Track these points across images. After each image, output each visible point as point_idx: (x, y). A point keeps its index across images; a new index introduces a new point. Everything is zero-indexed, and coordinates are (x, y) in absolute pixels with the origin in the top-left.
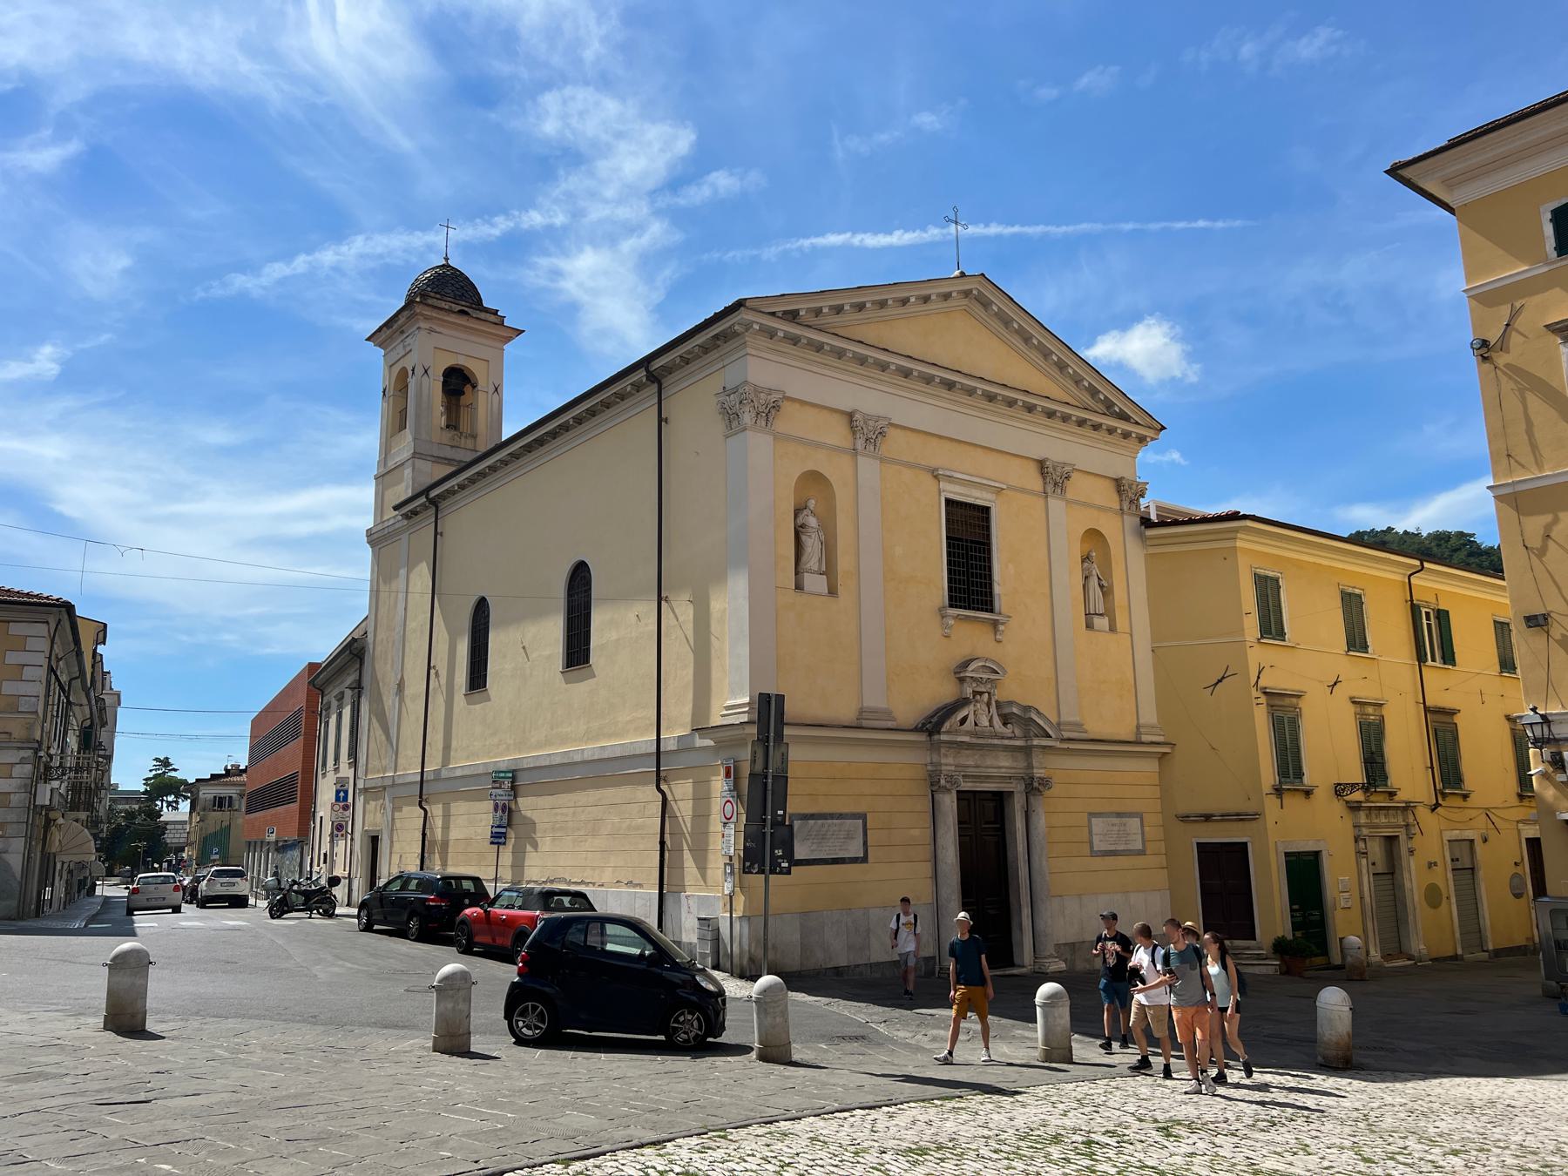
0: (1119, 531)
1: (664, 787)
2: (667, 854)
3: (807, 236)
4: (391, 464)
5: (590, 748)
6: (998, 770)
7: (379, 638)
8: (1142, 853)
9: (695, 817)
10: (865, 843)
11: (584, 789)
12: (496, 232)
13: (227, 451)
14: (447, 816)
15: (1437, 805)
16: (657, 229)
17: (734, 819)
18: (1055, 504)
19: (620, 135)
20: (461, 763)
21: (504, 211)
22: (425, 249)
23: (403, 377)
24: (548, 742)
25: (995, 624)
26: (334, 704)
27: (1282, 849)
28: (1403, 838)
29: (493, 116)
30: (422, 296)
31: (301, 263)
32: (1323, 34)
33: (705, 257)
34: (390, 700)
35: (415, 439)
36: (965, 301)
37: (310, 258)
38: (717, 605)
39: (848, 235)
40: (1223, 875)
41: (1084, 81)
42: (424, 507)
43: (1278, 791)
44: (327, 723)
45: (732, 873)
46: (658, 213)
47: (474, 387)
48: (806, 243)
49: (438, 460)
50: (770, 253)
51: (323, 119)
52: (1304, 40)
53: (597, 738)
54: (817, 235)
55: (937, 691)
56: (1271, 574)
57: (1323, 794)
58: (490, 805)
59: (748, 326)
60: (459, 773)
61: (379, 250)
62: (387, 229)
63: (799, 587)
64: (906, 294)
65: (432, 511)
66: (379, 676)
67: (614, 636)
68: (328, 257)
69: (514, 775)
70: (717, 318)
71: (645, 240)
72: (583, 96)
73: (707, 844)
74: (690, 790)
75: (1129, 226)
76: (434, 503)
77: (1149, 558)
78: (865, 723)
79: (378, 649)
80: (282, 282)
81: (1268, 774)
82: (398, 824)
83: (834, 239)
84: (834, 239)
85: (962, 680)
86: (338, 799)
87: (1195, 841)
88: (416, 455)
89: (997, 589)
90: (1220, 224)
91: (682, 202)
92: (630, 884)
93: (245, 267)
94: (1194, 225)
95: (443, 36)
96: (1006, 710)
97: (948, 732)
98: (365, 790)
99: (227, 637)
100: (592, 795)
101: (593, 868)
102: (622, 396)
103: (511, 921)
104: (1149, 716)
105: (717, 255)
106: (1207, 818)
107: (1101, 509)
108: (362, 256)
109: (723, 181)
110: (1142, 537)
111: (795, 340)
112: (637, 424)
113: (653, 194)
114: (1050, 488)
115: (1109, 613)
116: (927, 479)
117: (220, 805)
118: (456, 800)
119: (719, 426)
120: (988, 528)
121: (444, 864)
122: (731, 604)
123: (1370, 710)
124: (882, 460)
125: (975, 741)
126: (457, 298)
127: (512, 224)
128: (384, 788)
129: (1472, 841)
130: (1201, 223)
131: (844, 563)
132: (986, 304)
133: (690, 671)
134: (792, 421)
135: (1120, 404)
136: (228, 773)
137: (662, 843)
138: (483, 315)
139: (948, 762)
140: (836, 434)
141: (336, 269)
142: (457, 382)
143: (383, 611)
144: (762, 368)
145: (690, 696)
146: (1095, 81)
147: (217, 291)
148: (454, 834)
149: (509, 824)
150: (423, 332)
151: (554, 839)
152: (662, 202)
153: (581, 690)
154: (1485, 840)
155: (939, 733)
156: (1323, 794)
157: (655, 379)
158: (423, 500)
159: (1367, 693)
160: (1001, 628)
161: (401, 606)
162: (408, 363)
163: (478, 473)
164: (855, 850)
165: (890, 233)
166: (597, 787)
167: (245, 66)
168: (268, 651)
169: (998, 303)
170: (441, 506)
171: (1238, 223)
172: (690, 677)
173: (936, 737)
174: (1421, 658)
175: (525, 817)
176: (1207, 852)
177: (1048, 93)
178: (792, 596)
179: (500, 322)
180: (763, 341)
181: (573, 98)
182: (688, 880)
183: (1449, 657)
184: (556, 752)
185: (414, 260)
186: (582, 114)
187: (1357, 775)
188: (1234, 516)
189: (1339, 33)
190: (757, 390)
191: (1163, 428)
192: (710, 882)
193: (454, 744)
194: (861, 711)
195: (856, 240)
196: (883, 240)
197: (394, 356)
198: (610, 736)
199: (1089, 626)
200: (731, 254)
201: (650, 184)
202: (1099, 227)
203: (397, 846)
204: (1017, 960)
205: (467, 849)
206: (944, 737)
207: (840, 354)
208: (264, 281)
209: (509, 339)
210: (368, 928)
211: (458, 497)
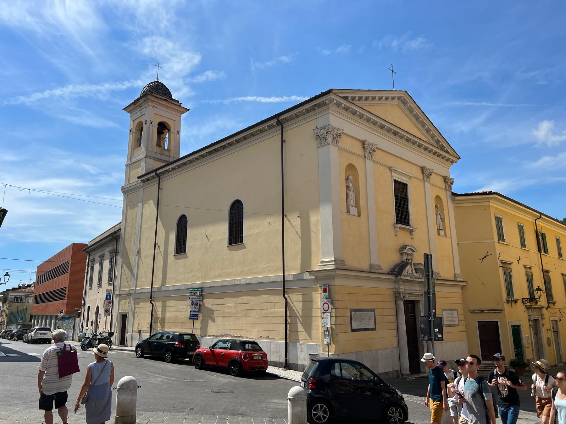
0: (444, 196)
1: (286, 296)
2: (288, 326)
3: (241, 97)
4: (134, 160)
5: (244, 279)
6: (415, 291)
7: (127, 231)
8: (458, 325)
9: (303, 309)
10: (375, 322)
11: (240, 296)
12: (124, 87)
13: (12, 163)
14: (164, 307)
15: (548, 307)
17: (329, 311)
18: (427, 184)
19: (173, 55)
20: (171, 284)
21: (128, 80)
23: (140, 128)
24: (220, 276)
25: (411, 232)
26: (97, 259)
27: (511, 324)
28: (540, 319)
29: (125, 45)
30: (151, 92)
31: (47, 93)
32: (420, 40)
33: (203, 101)
34: (133, 258)
35: (146, 150)
36: (398, 101)
37: (51, 92)
38: (313, 218)
39: (255, 97)
40: (489, 335)
41: (339, 49)
42: (153, 177)
43: (508, 301)
44: (92, 268)
45: (329, 335)
46: (186, 84)
47: (169, 130)
48: (240, 99)
49: (156, 159)
50: (227, 102)
51: (59, 41)
53: (247, 274)
54: (244, 97)
55: (394, 259)
56: (499, 216)
57: (520, 302)
58: (189, 302)
59: (331, 101)
60: (171, 289)
61: (78, 91)
62: (82, 83)
63: (348, 212)
64: (382, 95)
65: (158, 178)
66: (127, 247)
67: (256, 231)
68: (58, 92)
69: (202, 290)
70: (317, 97)
72: (159, 40)
73: (311, 321)
74: (301, 297)
76: (158, 176)
77: (456, 208)
78: (373, 271)
79: (127, 236)
80: (39, 100)
81: (505, 296)
82: (137, 310)
83: (250, 98)
84: (250, 98)
85: (402, 254)
86: (107, 299)
87: (477, 320)
88: (147, 156)
89: (411, 217)
92: (267, 338)
93: (24, 94)
95: (107, 14)
96: (417, 267)
97: (404, 276)
98: (120, 295)
99: (10, 235)
100: (245, 299)
101: (246, 330)
102: (261, 131)
103: (226, 356)
104: (458, 271)
105: (207, 101)
106: (482, 311)
107: (440, 188)
108: (72, 93)
109: (210, 75)
110: (453, 201)
111: (346, 109)
112: (271, 142)
113: (185, 77)
114: (425, 178)
115: (444, 229)
116: (387, 170)
117: (17, 300)
118: (169, 300)
119: (314, 143)
120: (406, 192)
121: (163, 327)
122: (322, 219)
123: (528, 270)
124: (374, 161)
125: (412, 279)
126: (163, 95)
127: (130, 85)
128: (130, 294)
129: (556, 321)
131: (362, 203)
132: (404, 103)
133: (299, 246)
134: (345, 142)
135: (447, 148)
136: (20, 287)
137: (286, 320)
138: (172, 101)
139: (403, 288)
140: (358, 149)
141: (61, 97)
142: (163, 128)
143: (129, 220)
144: (335, 119)
145: (299, 257)
147: (13, 102)
148: (168, 315)
149: (199, 311)
151: (224, 317)
153: (238, 254)
154: (560, 320)
155: (401, 275)
156: (520, 302)
158: (154, 174)
159: (528, 264)
160: (414, 233)
161: (139, 219)
162: (143, 119)
163: (183, 163)
164: (372, 325)
165: (270, 98)
166: (248, 295)
167: (29, 19)
168: (27, 240)
169: (410, 103)
172: (300, 249)
173: (399, 277)
174: (540, 251)
175: (207, 308)
178: (345, 216)
179: (180, 105)
180: (335, 108)
181: (156, 41)
183: (546, 251)
184: (225, 280)
185: (92, 95)
186: (159, 46)
187: (527, 296)
188: (490, 193)
189: (425, 40)
190: (334, 128)
191: (460, 158)
192: (313, 338)
193: (168, 276)
194: (371, 265)
195: (258, 99)
196: (267, 100)
197: (135, 116)
198: (255, 274)
199: (439, 234)
203: (136, 320)
204: (422, 370)
205: (176, 320)
206: (402, 277)
207: (361, 116)
208: (32, 99)
209: (184, 112)
210: (142, 356)
211: (170, 173)
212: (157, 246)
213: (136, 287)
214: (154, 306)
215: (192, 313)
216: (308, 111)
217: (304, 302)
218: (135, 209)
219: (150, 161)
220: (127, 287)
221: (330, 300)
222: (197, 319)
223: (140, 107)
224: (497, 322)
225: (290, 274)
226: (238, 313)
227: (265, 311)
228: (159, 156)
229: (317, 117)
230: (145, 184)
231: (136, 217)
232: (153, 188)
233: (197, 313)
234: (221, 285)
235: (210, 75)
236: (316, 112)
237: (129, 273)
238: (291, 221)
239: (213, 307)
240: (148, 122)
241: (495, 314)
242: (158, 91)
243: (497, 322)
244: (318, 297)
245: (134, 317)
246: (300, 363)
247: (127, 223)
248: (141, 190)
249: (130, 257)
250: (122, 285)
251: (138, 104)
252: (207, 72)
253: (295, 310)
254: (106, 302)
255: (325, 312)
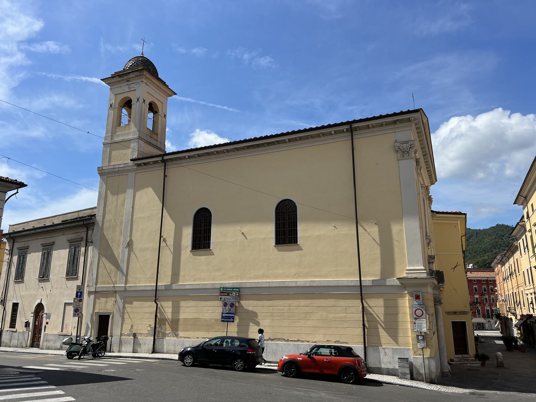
2: (366, 330)
3: (85, 76)
9: (386, 314)
16: (19, 58)
19: (8, 16)
20: (187, 281)
22: (138, 50)
24: (263, 277)
33: (39, 73)
38: (395, 228)
41: (195, 50)
45: (423, 339)
46: (20, 50)
48: (84, 78)
50: (68, 78)
52: (262, 59)
53: (306, 276)
54: (89, 77)
58: (220, 303)
71: (13, 60)
75: (203, 103)
79: (106, 225)
82: (129, 310)
86: (77, 296)
87: (451, 321)
88: (139, 138)
90: (231, 109)
91: (32, 49)
94: (223, 107)
100: (303, 302)
105: (44, 74)
106: (455, 313)
109: (52, 46)
113: (21, 42)
128: (116, 292)
130: (225, 108)
137: (364, 325)
145: (379, 262)
146: (198, 51)
150: (144, 84)
152: (22, 47)
157: (351, 131)
158: (160, 158)
163: (207, 153)
170: (167, 164)
171: (236, 110)
176: (454, 324)
177: (182, 51)
182: (383, 341)
189: (273, 60)
198: (316, 276)
200: (51, 75)
201: (20, 39)
202: (193, 101)
203: (127, 321)
212: (162, 239)
213: (126, 283)
214: (159, 305)
215: (224, 315)
216: (387, 124)
217: (386, 307)
218: (121, 197)
219: (142, 143)
220: (109, 284)
221: (424, 306)
222: (233, 321)
223: (129, 81)
224: (465, 322)
225: (367, 279)
226: (294, 317)
227: (333, 315)
228: (149, 140)
229: (396, 131)
230: (140, 168)
231: (123, 204)
232: (157, 173)
233: (233, 315)
234: (267, 286)
235: (52, 46)
236: (396, 126)
237: (113, 268)
238: (365, 227)
239: (255, 310)
240: (141, 100)
241: (463, 315)
242: (144, 67)
243: (465, 322)
244: (406, 303)
245: (123, 319)
246: (383, 366)
247: (107, 209)
248: (131, 175)
249: (114, 249)
250: (99, 281)
251: (125, 77)
252: (49, 42)
253: (375, 315)
254: (76, 300)
255: (418, 317)
